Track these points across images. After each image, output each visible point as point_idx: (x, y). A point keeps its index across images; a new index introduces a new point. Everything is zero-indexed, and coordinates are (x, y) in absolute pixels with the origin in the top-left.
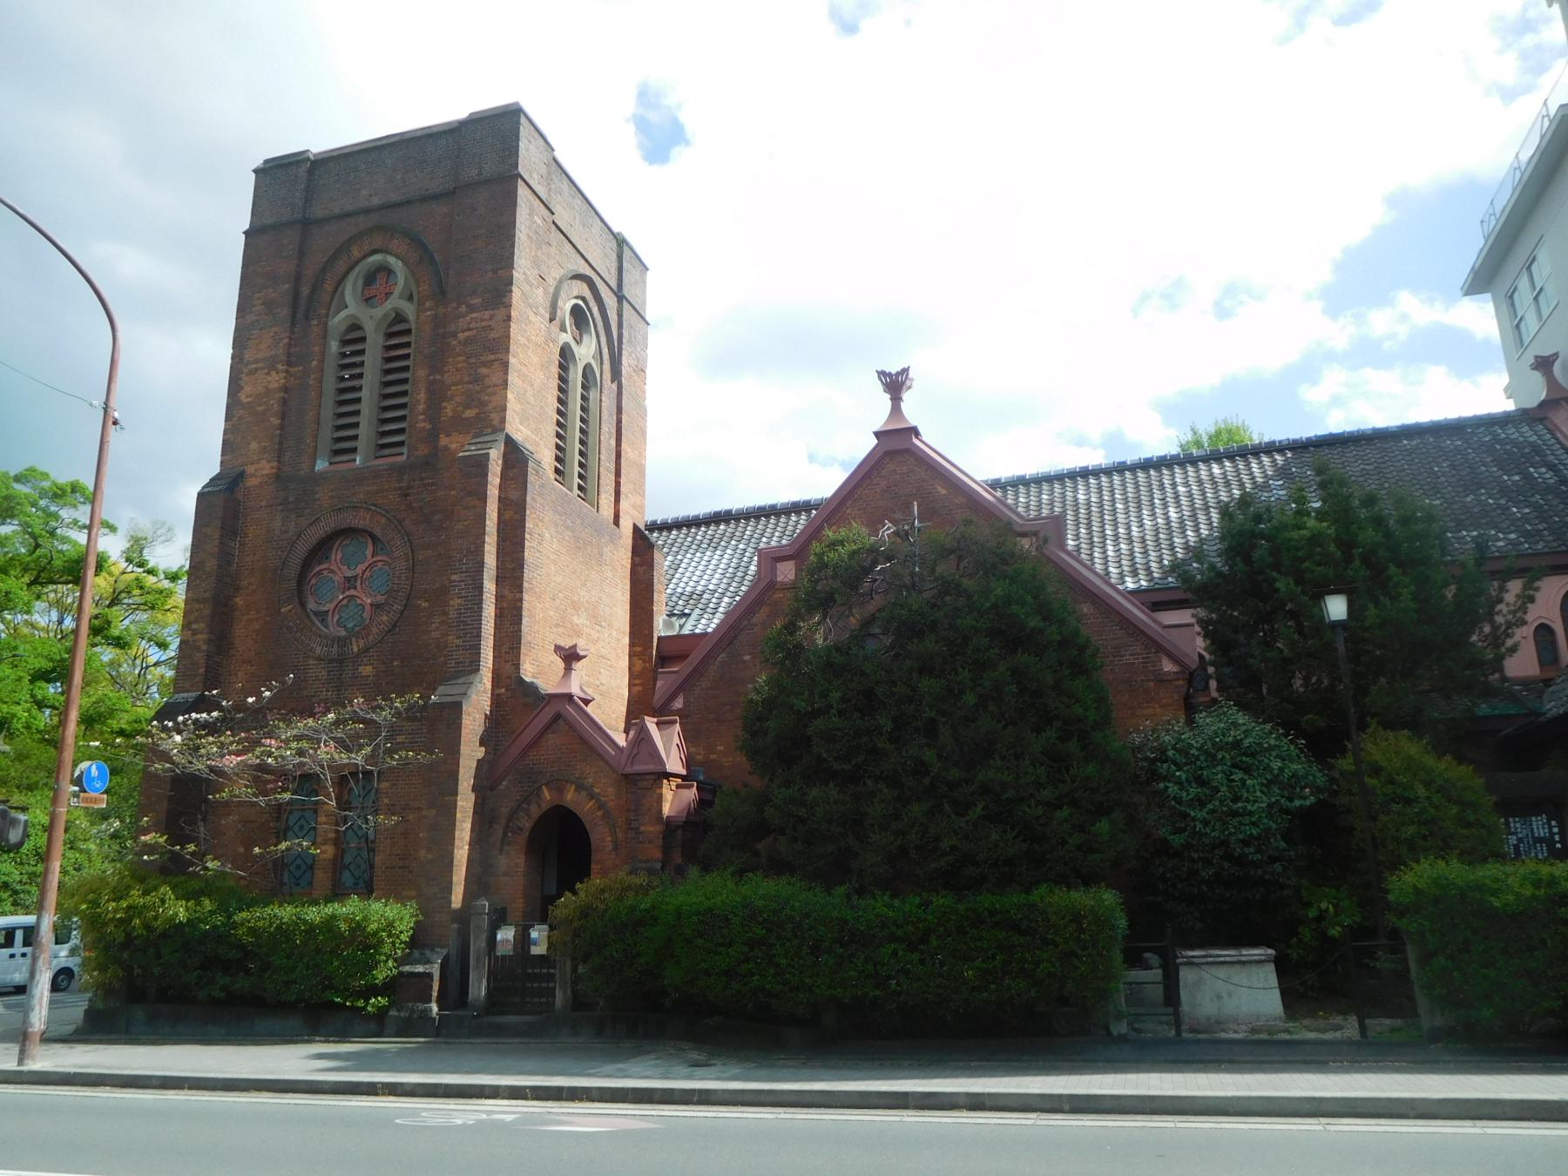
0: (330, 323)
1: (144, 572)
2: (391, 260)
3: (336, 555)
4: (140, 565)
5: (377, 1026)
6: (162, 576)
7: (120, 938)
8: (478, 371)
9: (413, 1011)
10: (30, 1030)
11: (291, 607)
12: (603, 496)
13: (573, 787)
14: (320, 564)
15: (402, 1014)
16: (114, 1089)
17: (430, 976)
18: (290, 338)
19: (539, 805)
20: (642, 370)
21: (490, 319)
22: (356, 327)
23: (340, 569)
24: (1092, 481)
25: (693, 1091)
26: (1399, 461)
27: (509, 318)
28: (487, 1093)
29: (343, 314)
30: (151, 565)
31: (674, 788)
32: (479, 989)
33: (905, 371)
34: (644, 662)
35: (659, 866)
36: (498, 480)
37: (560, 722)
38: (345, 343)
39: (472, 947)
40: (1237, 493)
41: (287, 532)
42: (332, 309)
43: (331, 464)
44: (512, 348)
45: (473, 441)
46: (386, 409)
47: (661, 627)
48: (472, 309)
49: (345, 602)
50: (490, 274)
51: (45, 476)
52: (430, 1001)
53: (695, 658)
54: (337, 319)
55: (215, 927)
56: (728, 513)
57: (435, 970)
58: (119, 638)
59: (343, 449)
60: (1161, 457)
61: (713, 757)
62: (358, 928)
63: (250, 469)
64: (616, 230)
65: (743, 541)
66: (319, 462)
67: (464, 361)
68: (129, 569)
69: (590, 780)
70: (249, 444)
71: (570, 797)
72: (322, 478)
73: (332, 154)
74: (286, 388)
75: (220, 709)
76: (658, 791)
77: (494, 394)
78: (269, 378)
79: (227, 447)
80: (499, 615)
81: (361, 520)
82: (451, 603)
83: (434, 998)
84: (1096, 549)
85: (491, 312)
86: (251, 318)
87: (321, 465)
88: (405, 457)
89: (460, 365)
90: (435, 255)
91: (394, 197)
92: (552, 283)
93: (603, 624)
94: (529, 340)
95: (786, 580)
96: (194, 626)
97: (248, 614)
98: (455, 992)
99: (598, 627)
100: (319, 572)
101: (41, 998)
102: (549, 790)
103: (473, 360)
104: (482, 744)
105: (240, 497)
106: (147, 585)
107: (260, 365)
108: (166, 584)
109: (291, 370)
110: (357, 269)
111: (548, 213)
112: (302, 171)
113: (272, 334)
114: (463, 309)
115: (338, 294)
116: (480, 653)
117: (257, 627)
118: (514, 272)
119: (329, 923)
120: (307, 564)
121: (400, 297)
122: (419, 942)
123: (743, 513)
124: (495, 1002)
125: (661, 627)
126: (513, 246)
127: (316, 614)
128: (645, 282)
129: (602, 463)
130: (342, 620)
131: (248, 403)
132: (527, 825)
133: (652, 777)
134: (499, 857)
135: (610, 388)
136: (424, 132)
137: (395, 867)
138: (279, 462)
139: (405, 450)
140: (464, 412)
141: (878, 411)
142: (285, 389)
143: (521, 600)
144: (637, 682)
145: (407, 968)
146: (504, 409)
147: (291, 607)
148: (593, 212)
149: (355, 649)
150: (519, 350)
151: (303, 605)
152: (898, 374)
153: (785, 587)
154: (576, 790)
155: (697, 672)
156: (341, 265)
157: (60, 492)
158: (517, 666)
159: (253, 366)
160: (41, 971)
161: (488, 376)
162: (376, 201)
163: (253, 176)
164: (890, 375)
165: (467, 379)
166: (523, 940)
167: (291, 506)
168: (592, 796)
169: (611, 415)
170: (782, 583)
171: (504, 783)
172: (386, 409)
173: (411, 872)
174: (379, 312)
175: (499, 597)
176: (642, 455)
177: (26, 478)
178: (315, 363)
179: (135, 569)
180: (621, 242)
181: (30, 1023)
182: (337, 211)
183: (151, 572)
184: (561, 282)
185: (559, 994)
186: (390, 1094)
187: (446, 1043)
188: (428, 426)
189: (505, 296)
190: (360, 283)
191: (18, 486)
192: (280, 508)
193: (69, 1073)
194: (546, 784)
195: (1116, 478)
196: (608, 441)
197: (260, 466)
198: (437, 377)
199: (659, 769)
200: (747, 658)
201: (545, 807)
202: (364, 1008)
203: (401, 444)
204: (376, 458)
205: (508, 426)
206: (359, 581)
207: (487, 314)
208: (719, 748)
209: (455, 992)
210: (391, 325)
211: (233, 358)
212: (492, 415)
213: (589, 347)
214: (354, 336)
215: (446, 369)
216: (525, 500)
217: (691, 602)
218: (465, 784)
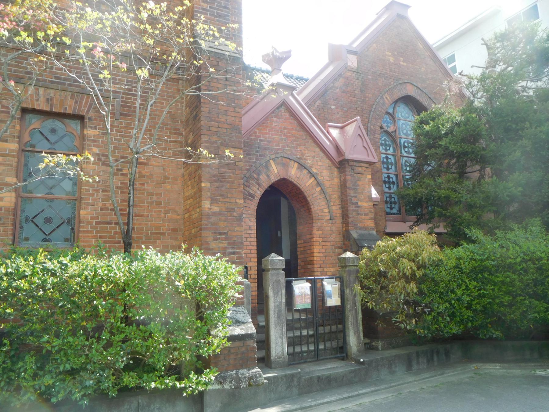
9: (239, 380)
15: (227, 386)
19: (268, 176)
26: (381, 111)
69: (310, 162)
95: (352, 66)
102: (277, 164)
132: (259, 192)
137: (109, 223)
154: (298, 168)
168: (312, 175)
200: (333, 107)
201: (273, 179)
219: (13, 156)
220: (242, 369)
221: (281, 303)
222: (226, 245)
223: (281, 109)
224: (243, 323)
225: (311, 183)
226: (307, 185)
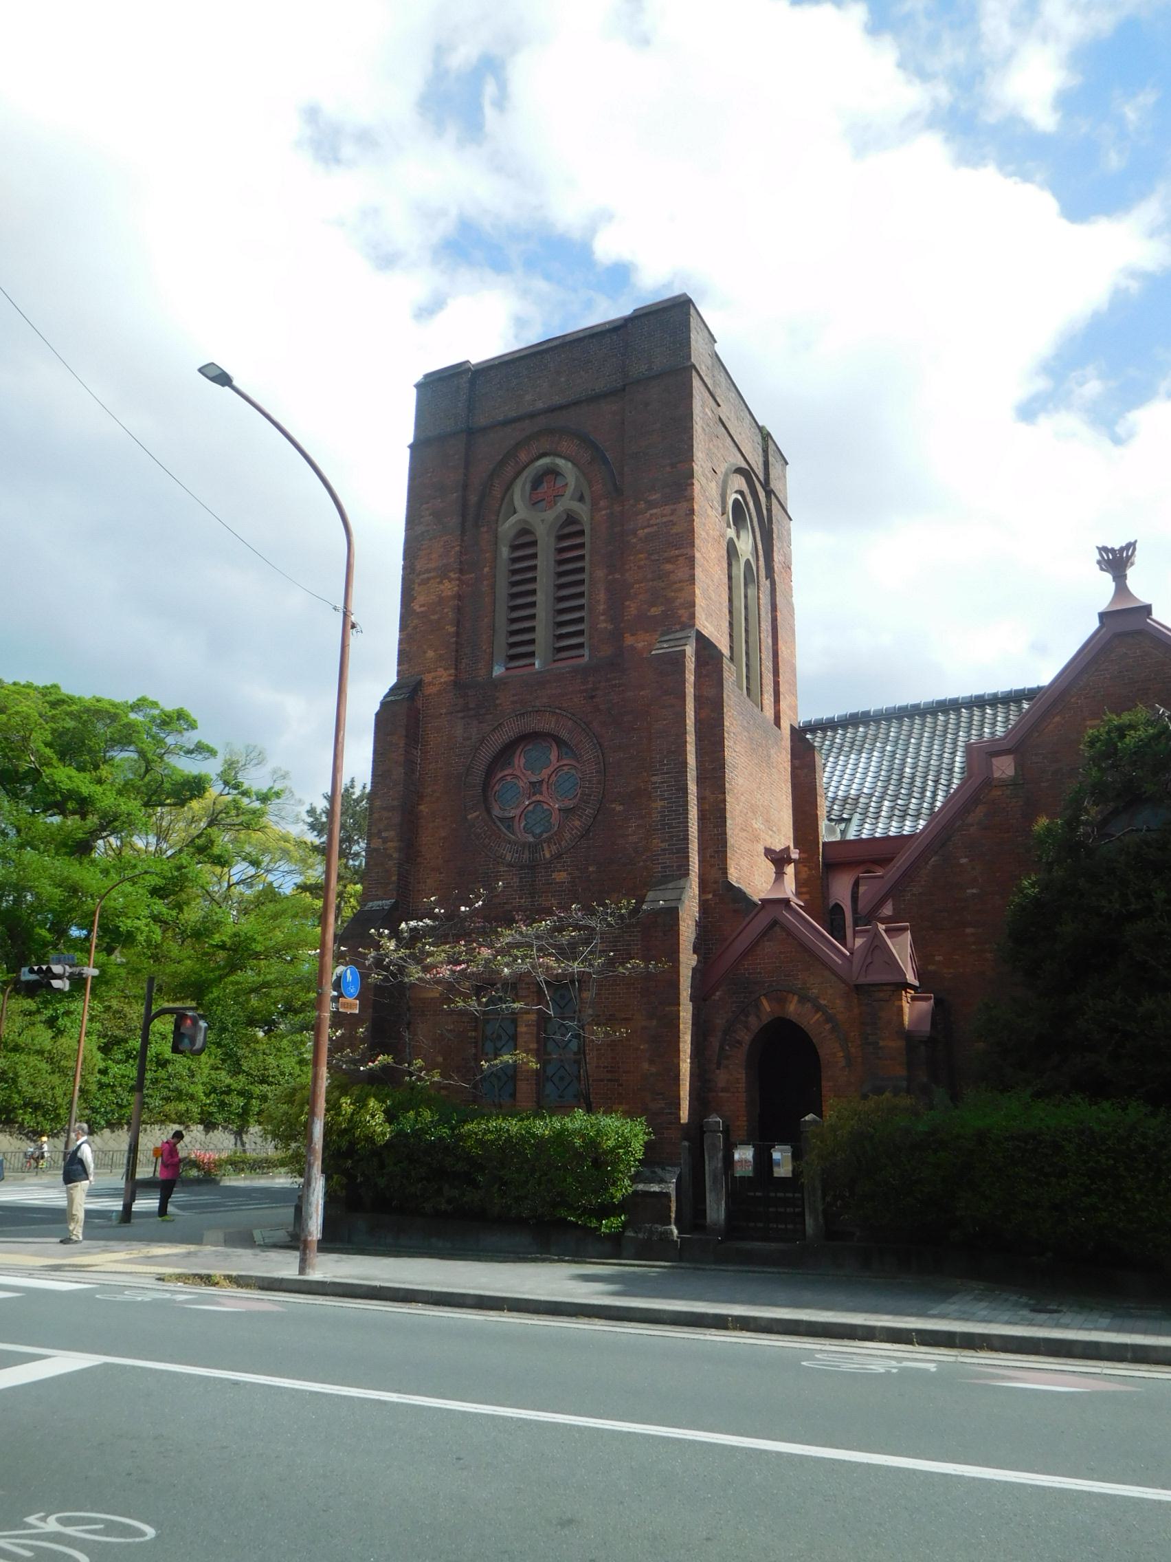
0: (499, 530)
1: (239, 793)
2: (561, 462)
3: (519, 761)
4: (236, 787)
5: (613, 1248)
6: (254, 798)
7: (344, 1144)
8: (662, 567)
10: (310, 1238)
11: (478, 813)
12: (766, 696)
13: (796, 998)
14: (502, 770)
15: (640, 1236)
16: (428, 1307)
17: (667, 1195)
18: (460, 545)
19: (758, 1017)
20: (788, 567)
21: (672, 514)
22: (525, 531)
23: (524, 775)
24: (988, 711)
25: (1125, 1346)
27: (692, 511)
28: (860, 1333)
29: (513, 519)
30: (245, 787)
31: (909, 1000)
32: (716, 1210)
33: (1131, 546)
34: (810, 869)
35: (904, 1084)
36: (693, 678)
37: (777, 929)
38: (514, 548)
39: (707, 1167)
40: (974, 739)
41: (471, 739)
42: (501, 515)
43: (507, 669)
44: (697, 542)
45: (663, 639)
46: (561, 612)
47: (827, 833)
48: (651, 505)
49: (530, 808)
50: (668, 469)
51: (155, 704)
52: (670, 1224)
53: (902, 861)
54: (507, 525)
55: (441, 1139)
56: (866, 714)
57: (671, 1188)
58: (220, 857)
59: (519, 653)
60: (929, 703)
61: (931, 968)
62: (592, 1144)
63: (428, 678)
64: (760, 424)
65: (889, 743)
66: (496, 668)
67: (646, 559)
68: (226, 791)
70: (425, 652)
71: (793, 1008)
72: (501, 683)
73: (492, 363)
74: (460, 595)
75: (433, 917)
76: (897, 1003)
77: (681, 590)
78: (442, 587)
79: (404, 656)
80: (702, 818)
81: (547, 724)
82: (654, 805)
83: (673, 1220)
84: (940, 786)
85: (673, 507)
86: (420, 529)
87: (498, 671)
88: (586, 659)
89: (642, 563)
90: (606, 454)
91: (558, 400)
92: (721, 476)
93: (774, 829)
94: (708, 534)
95: (1004, 776)
96: (384, 834)
97: (434, 821)
98: (693, 1217)
99: (770, 833)
100: (502, 778)
101: (317, 1205)
103: (655, 557)
104: (695, 952)
105: (419, 704)
106: (243, 805)
107: (432, 574)
108: (257, 805)
109: (463, 578)
110: (525, 474)
111: (715, 406)
112: (465, 378)
113: (442, 543)
114: (642, 505)
115: (506, 500)
116: (688, 857)
117: (443, 835)
118: (694, 464)
119: (560, 1137)
120: (490, 771)
121: (572, 499)
122: (654, 1158)
123: (882, 714)
124: (735, 1227)
125: (827, 833)
126: (691, 438)
127: (501, 819)
128: (785, 477)
129: (763, 662)
130: (529, 826)
131: (422, 612)
133: (889, 988)
134: (718, 1071)
135: (765, 583)
136: (587, 333)
137: (602, 1080)
138: (456, 669)
139: (586, 652)
140: (649, 610)
141: (1102, 590)
142: (459, 597)
143: (724, 801)
144: (804, 890)
145: (641, 1187)
146: (693, 605)
147: (478, 813)
148: (744, 406)
149: (548, 856)
150: (701, 545)
151: (488, 811)
152: (1122, 549)
153: (1003, 784)
154: (799, 1001)
155: (908, 876)
156: (509, 471)
157: (168, 720)
158: (724, 871)
159: (426, 576)
160: (316, 1179)
161: (673, 572)
162: (540, 405)
163: (415, 391)
164: (1113, 550)
165: (650, 576)
166: (763, 1161)
167: (472, 713)
168: (818, 1008)
169: (767, 613)
170: (999, 779)
171: (718, 993)
172: (561, 612)
173: (621, 1085)
174: (550, 515)
175: (701, 799)
176: (793, 655)
177: (139, 707)
178: (486, 570)
179: (231, 791)
180: (766, 437)
181: (309, 1232)
182: (501, 418)
183: (245, 793)
184: (726, 475)
185: (809, 1222)
186: (742, 1329)
187: (694, 1269)
188: (610, 627)
189: (686, 489)
190: (528, 487)
191: (132, 716)
192: (460, 715)
193: (376, 1286)
194: (764, 995)
195: (977, 712)
196: (767, 641)
197: (437, 673)
198: (617, 576)
199: (904, 981)
200: (964, 861)
201: (766, 1019)
202: (597, 1229)
203: (581, 646)
204: (555, 661)
205: (697, 622)
206: (545, 786)
207: (668, 509)
208: (937, 958)
209: (693, 1217)
210: (563, 526)
211: (404, 568)
212: (679, 612)
213: (747, 543)
214: (524, 541)
215: (627, 567)
216: (723, 697)
217: (847, 806)
218: (685, 994)
219: (533, 1025)
220: (657, 1223)
221: (716, 1168)
222: (663, 1106)
223: (775, 929)
224: (666, 1182)
225: (818, 1019)
226: (812, 1022)
